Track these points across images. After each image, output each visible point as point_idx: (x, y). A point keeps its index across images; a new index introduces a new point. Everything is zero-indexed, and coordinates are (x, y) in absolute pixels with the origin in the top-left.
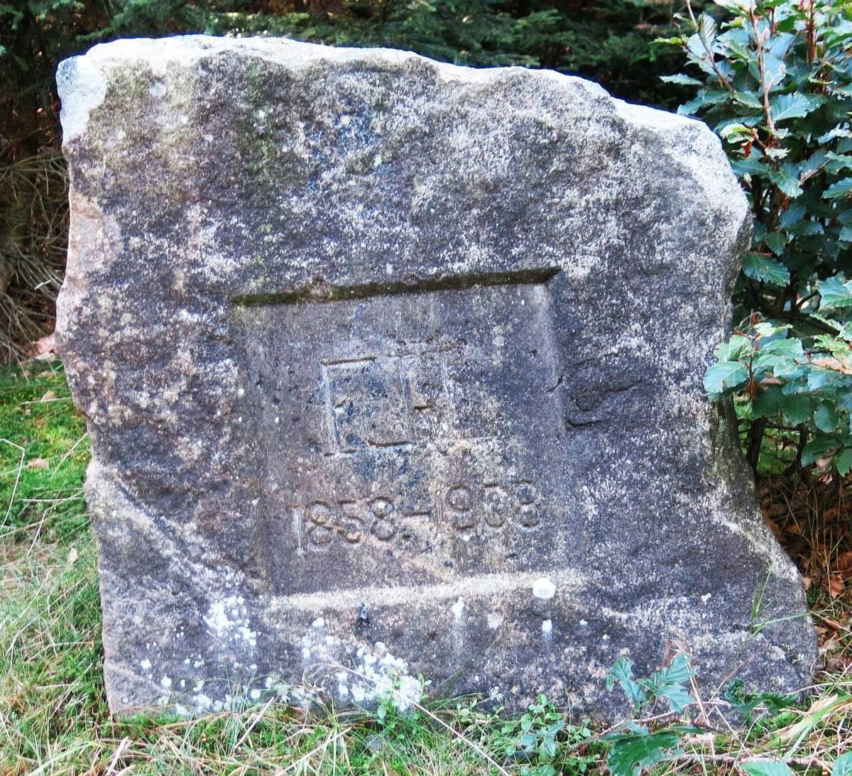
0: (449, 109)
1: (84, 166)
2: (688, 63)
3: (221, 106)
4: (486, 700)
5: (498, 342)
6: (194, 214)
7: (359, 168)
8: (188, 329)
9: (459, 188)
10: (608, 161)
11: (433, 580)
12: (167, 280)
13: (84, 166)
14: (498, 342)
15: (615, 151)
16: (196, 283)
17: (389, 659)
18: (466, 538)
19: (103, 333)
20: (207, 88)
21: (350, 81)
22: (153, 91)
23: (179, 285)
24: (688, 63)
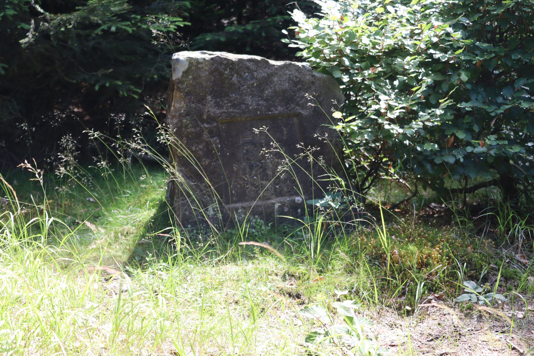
0: (487, 331)
1: (180, 85)
2: (290, 13)
3: (216, 70)
4: (175, 87)
5: (285, 132)
6: (209, 98)
7: (251, 86)
8: (206, 128)
9: (275, 91)
10: (311, 85)
11: (269, 199)
12: (201, 115)
13: (180, 85)
14: (285, 132)
15: (313, 83)
16: (209, 116)
17: (259, 220)
18: (277, 187)
19: (183, 129)
20: (213, 65)
21: (248, 64)
22: (199, 66)
23: (205, 117)
24: (290, 13)
